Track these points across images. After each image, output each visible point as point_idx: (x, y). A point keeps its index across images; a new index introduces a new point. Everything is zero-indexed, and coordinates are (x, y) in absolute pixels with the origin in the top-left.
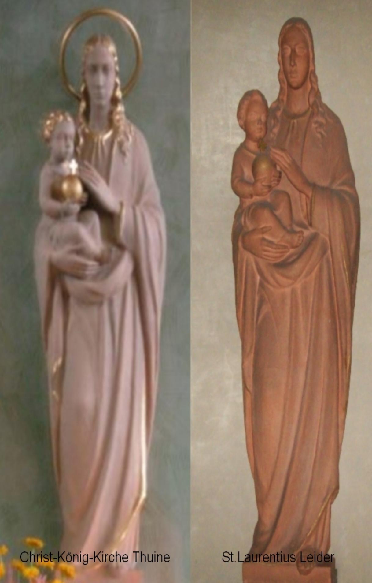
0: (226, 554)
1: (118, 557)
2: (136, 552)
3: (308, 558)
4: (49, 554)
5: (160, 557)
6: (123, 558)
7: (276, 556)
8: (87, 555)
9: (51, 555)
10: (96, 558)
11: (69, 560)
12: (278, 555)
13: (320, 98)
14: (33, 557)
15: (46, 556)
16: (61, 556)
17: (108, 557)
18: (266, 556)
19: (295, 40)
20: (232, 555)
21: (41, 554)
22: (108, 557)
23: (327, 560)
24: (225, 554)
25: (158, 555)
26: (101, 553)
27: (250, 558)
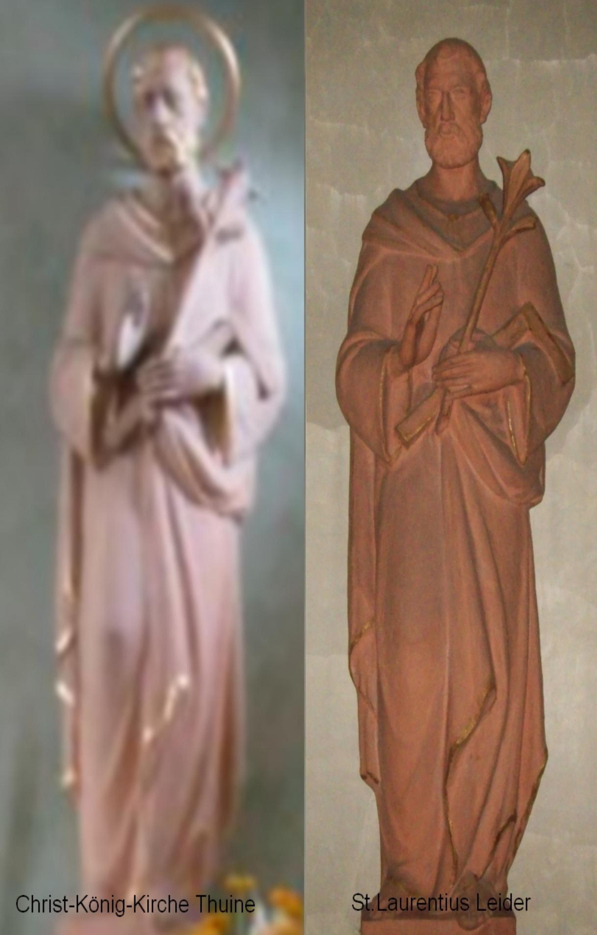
0: (358, 898)
1: (173, 904)
2: (201, 896)
3: (489, 904)
4: (61, 899)
5: (239, 904)
6: (246, 906)
7: (438, 901)
8: (123, 901)
9: (65, 900)
10: (80, 906)
11: (94, 909)
12: (441, 898)
13: (548, 435)
14: (36, 904)
15: (57, 903)
16: (138, 903)
17: (156, 904)
18: (422, 901)
19: (453, 87)
20: (65, 900)
21: (49, 899)
22: (156, 904)
23: (504, 908)
24: (357, 898)
25: (236, 901)
26: (146, 899)
27: (396, 903)
